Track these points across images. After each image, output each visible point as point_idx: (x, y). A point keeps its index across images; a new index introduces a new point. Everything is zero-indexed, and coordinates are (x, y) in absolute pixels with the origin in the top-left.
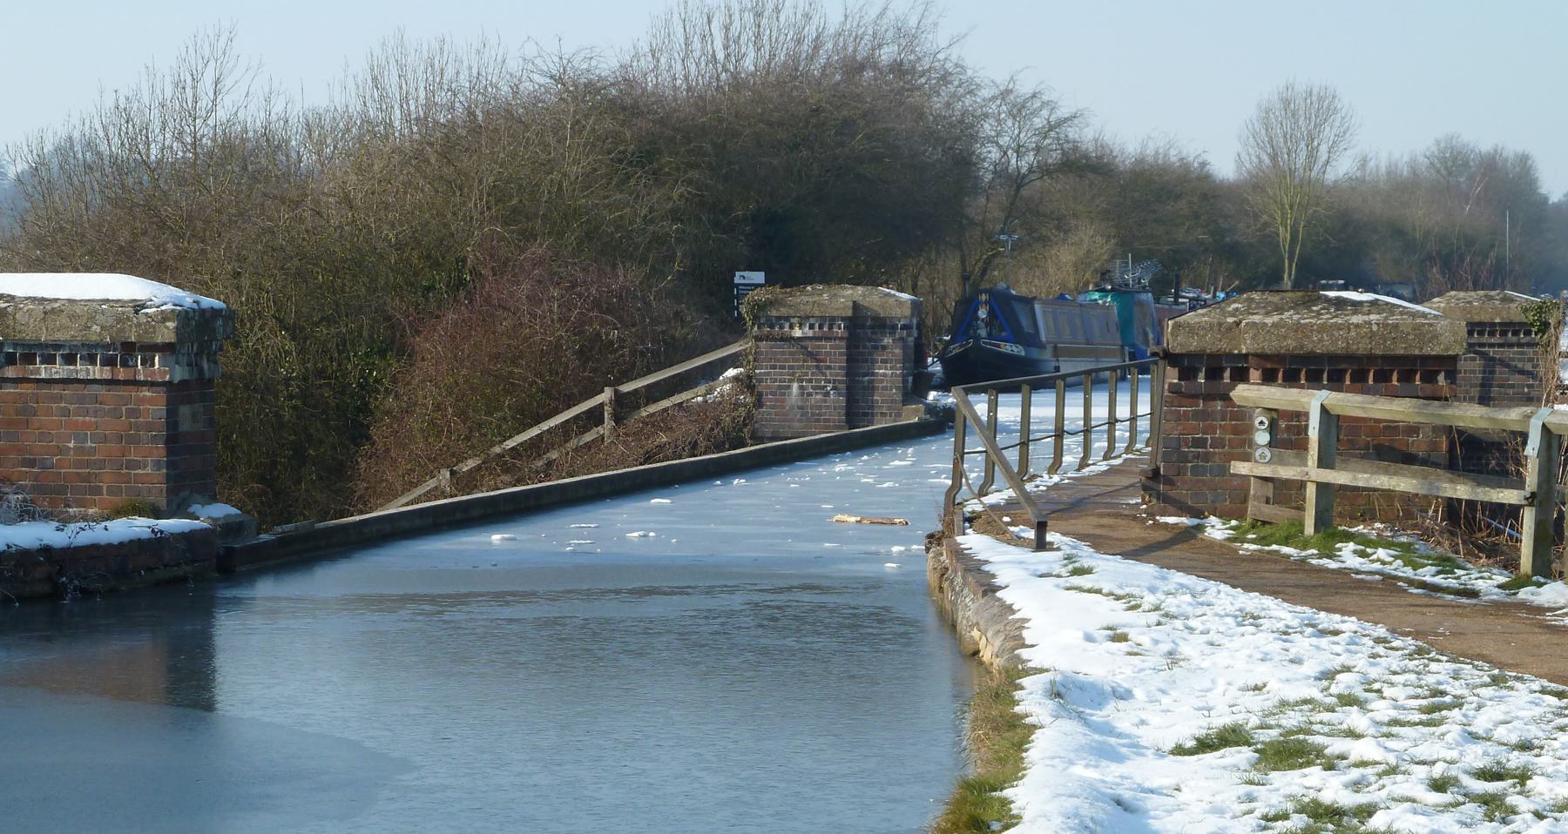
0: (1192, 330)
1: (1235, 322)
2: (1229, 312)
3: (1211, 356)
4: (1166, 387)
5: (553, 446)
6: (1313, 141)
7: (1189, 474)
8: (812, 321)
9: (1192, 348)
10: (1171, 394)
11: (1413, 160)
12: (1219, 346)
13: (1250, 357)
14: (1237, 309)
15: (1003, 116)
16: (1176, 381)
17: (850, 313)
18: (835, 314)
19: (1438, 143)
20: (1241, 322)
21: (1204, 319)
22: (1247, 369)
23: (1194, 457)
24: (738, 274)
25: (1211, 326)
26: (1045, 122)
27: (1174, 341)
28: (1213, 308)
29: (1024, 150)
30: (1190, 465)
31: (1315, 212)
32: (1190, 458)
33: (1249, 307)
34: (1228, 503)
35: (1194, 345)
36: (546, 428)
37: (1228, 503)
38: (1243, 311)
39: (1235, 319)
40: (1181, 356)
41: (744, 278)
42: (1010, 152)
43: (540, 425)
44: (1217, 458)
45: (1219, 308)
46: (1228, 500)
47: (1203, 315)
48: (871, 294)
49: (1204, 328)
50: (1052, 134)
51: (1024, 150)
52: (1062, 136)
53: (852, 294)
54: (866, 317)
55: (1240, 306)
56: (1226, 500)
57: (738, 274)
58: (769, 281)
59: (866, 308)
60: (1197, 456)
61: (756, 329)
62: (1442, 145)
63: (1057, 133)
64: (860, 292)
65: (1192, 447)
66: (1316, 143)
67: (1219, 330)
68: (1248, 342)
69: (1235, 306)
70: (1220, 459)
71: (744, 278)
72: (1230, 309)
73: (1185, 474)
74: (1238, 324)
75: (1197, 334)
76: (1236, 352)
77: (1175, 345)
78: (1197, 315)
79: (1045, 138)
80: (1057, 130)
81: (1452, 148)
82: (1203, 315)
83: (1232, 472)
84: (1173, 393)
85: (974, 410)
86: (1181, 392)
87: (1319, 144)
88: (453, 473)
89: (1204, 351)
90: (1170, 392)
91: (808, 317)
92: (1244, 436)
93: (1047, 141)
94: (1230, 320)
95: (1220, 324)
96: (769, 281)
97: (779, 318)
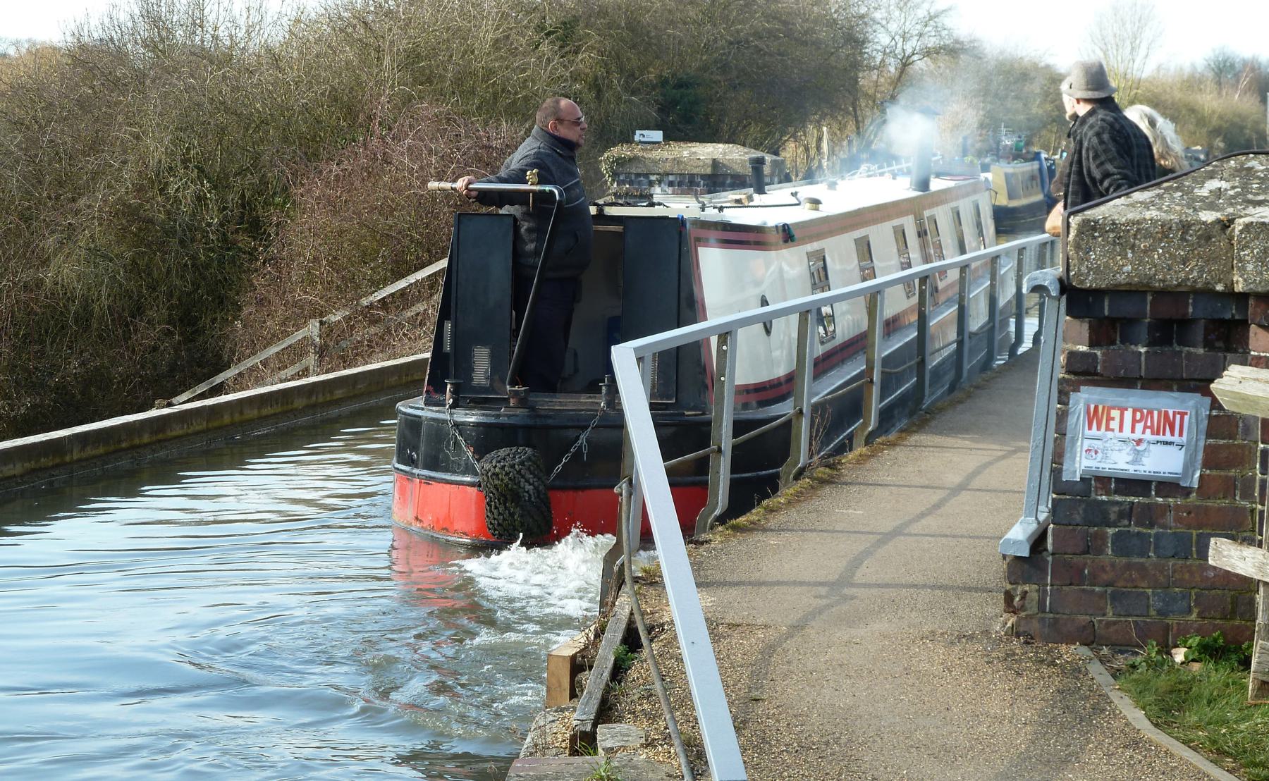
0: (1120, 236)
1: (1219, 221)
2: (1203, 199)
3: (1164, 294)
4: (1062, 359)
5: (418, 299)
6: (1136, 39)
7: (1110, 552)
8: (671, 178)
9: (1121, 278)
10: (1072, 377)
11: (1193, 66)
12: (1182, 275)
13: (1251, 302)
14: (1218, 193)
15: (892, 8)
16: (1083, 348)
17: (709, 171)
18: (695, 171)
19: (1214, 50)
20: (1231, 221)
21: (1148, 215)
22: (1244, 324)
23: (1121, 515)
24: (638, 132)
25: (1166, 228)
26: (926, 13)
27: (1081, 260)
28: (1166, 189)
29: (909, 35)
30: (1111, 531)
31: (1136, 93)
32: (1113, 517)
33: (1245, 187)
34: (1194, 616)
35: (1125, 270)
36: (413, 281)
37: (1194, 616)
38: (1233, 197)
39: (1218, 215)
40: (1098, 293)
41: (644, 136)
42: (897, 38)
43: (408, 278)
44: (1170, 519)
45: (1177, 189)
46: (1196, 611)
47: (1146, 205)
48: (731, 152)
49: (1148, 235)
50: (931, 23)
51: (909, 35)
52: (939, 25)
53: (712, 152)
54: (725, 175)
55: (1224, 185)
56: (1190, 611)
57: (638, 132)
58: (667, 138)
59: (724, 165)
60: (1127, 513)
61: (615, 185)
62: (1217, 52)
63: (936, 22)
64: (720, 150)
65: (1116, 492)
66: (1138, 42)
67: (1183, 239)
68: (1250, 267)
69: (1214, 184)
70: (1178, 520)
71: (644, 136)
72: (1204, 192)
73: (1100, 551)
74: (1226, 225)
75: (1133, 247)
76: (1219, 287)
77: (1084, 269)
78: (1132, 205)
79: (926, 26)
80: (936, 20)
81: (1224, 54)
82: (1146, 205)
83: (1211, 562)
84: (1075, 373)
85: (908, 215)
86: (1096, 374)
87: (1140, 42)
88: (322, 323)
89: (1148, 285)
90: (1068, 372)
91: (668, 174)
92: (1232, 473)
93: (928, 29)
94: (1208, 216)
95: (1185, 227)
96: (667, 138)
97: (638, 175)
